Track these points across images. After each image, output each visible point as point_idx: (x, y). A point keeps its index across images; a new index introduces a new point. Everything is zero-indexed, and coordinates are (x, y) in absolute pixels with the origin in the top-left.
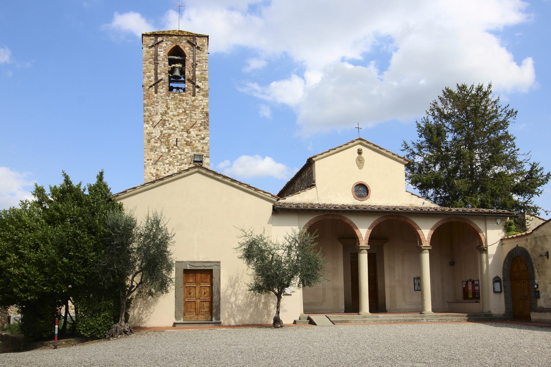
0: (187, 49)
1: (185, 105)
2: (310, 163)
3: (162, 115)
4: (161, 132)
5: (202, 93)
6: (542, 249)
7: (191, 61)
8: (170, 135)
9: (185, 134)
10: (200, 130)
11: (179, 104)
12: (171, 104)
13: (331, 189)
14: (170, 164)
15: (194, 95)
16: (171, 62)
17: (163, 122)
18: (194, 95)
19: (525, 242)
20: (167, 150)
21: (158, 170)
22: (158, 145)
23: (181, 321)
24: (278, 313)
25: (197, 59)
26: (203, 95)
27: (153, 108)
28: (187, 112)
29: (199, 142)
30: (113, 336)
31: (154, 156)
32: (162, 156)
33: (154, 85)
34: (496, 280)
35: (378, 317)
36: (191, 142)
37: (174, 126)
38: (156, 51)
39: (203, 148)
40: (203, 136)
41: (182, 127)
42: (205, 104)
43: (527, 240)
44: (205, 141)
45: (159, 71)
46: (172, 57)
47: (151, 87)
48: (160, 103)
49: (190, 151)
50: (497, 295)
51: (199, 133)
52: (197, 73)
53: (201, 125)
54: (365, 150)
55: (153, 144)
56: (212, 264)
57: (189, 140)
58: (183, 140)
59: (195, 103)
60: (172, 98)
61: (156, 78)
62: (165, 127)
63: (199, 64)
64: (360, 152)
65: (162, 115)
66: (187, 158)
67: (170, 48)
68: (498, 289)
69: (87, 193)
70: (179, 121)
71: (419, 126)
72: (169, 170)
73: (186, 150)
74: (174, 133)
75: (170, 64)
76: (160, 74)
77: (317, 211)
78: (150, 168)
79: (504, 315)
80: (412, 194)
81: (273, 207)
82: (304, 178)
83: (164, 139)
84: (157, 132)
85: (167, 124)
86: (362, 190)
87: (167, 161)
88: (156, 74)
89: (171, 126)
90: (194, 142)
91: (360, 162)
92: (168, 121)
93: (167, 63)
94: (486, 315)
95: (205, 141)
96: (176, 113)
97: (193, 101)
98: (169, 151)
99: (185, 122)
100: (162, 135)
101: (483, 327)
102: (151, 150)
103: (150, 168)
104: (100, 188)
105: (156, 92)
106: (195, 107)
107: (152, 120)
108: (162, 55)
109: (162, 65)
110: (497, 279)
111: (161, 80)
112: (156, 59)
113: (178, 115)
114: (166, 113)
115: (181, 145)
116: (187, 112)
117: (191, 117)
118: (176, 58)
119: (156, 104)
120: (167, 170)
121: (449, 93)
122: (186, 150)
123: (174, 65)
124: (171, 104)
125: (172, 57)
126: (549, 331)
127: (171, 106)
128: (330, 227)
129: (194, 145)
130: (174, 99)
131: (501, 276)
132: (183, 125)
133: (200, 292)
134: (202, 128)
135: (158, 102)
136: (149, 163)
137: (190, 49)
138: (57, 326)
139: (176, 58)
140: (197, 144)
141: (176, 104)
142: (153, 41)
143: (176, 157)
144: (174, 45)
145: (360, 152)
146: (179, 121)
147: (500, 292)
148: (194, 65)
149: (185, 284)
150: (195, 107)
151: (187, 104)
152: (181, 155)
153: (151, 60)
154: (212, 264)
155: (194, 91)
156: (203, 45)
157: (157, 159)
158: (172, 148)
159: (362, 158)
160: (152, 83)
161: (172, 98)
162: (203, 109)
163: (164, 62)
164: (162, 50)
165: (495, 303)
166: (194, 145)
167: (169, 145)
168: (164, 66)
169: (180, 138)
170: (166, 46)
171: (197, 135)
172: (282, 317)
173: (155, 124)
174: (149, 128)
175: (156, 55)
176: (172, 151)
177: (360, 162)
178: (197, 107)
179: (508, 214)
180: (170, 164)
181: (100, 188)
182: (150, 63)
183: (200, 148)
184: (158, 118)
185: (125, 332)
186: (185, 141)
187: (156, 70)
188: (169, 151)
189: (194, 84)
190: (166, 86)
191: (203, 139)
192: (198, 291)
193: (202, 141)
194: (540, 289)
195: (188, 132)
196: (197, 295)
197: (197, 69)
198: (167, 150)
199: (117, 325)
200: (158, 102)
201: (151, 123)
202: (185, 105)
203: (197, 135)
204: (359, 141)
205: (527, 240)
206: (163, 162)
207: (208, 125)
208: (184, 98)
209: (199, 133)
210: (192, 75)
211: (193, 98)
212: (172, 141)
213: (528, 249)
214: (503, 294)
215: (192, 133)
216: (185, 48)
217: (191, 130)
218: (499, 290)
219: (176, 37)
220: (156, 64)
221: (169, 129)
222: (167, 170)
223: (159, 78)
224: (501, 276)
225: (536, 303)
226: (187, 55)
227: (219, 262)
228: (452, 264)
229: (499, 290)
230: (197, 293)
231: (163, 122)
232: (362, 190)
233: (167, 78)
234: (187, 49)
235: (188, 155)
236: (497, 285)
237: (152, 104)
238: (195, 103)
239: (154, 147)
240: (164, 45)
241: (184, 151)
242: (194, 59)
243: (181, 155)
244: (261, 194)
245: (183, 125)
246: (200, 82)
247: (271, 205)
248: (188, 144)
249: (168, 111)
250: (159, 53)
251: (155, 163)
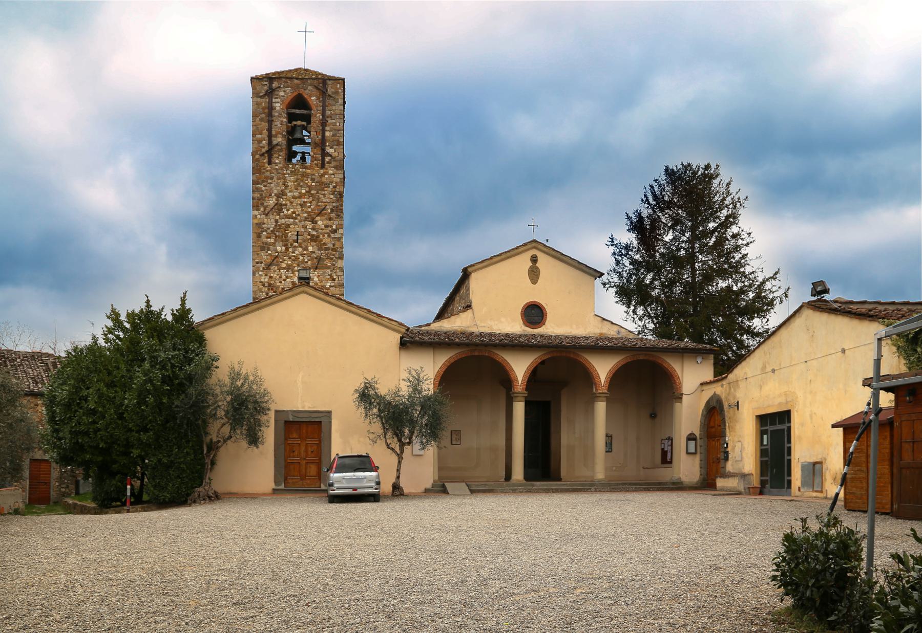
0: (314, 98)
1: (309, 182)
2: (466, 275)
3: (278, 196)
4: (277, 221)
5: (333, 164)
6: (734, 398)
7: (319, 116)
8: (288, 226)
9: (310, 225)
10: (330, 219)
11: (302, 181)
12: (291, 181)
13: (494, 311)
14: (289, 268)
15: (323, 166)
16: (291, 117)
17: (279, 208)
18: (323, 166)
19: (720, 388)
20: (284, 248)
21: (271, 277)
22: (272, 241)
23: (282, 487)
24: (398, 477)
25: (328, 113)
26: (336, 168)
27: (265, 186)
28: (313, 192)
29: (329, 236)
30: (195, 502)
31: (265, 257)
32: (277, 257)
33: (267, 152)
34: (691, 438)
35: (533, 486)
36: (318, 237)
37: (294, 212)
38: (271, 103)
39: (334, 245)
40: (334, 227)
41: (305, 215)
42: (338, 180)
43: (722, 386)
44: (337, 235)
45: (273, 133)
46: (293, 111)
47: (262, 155)
48: (275, 179)
49: (316, 249)
50: (691, 457)
51: (329, 223)
52: (327, 134)
53: (332, 211)
54: (541, 257)
55: (265, 240)
56: (321, 415)
57: (314, 233)
58: (306, 234)
59: (324, 179)
60: (292, 172)
61: (270, 142)
62: (282, 214)
63: (330, 121)
64: (534, 260)
65: (278, 196)
66: (312, 259)
67: (290, 98)
68: (692, 449)
69: (170, 318)
70: (301, 205)
71: (629, 218)
72: (287, 277)
73: (310, 249)
74: (295, 224)
75: (290, 121)
76: (276, 136)
77: (458, 345)
78: (261, 275)
79: (697, 483)
80: (604, 319)
81: (401, 338)
82: (456, 298)
83: (280, 232)
84: (270, 223)
85: (284, 210)
86: (534, 313)
87: (284, 265)
88: (270, 136)
89: (289, 212)
90: (321, 237)
91: (534, 274)
92: (286, 205)
93: (285, 120)
94: (674, 483)
95: (337, 235)
96: (296, 194)
97: (323, 175)
98: (287, 250)
99: (310, 207)
100: (278, 226)
101: (680, 499)
102: (262, 249)
103: (261, 275)
104: (183, 315)
105: (270, 163)
106: (322, 185)
107: (262, 204)
108: (278, 108)
109: (278, 124)
110: (692, 437)
111: (277, 145)
112: (270, 114)
113: (300, 197)
114: (283, 194)
115: (304, 241)
116: (313, 192)
117: (319, 199)
118: (297, 111)
119: (270, 181)
120: (284, 277)
121: (669, 172)
122: (310, 249)
123: (295, 123)
124: (291, 181)
125: (293, 111)
126: (920, 523)
127: (290, 184)
128: (473, 366)
129: (321, 240)
130: (293, 173)
131: (697, 433)
132: (307, 212)
133: (306, 451)
134: (333, 215)
135: (272, 178)
136: (259, 268)
137: (318, 98)
138: (129, 487)
139: (297, 111)
140: (326, 240)
141: (297, 179)
142: (266, 88)
143: (296, 258)
144: (296, 94)
145: (534, 260)
146: (301, 205)
147: (695, 453)
148: (324, 124)
149: (286, 439)
150: (322, 185)
151: (313, 180)
152: (303, 255)
153: (263, 116)
154: (321, 415)
155: (323, 160)
156: (337, 93)
157: (269, 261)
158: (292, 245)
159: (537, 268)
160: (264, 150)
161: (292, 172)
162: (335, 187)
163: (281, 119)
164: (278, 100)
165: (687, 467)
166: (321, 240)
167: (287, 241)
168: (280, 123)
169: (303, 230)
170: (285, 94)
171: (326, 226)
172: (403, 483)
173: (268, 209)
174: (259, 217)
175: (271, 108)
176: (291, 250)
177: (534, 274)
178: (327, 185)
179: (710, 350)
180: (289, 268)
181: (183, 315)
182: (261, 120)
183: (330, 245)
184: (272, 202)
185: (210, 498)
186: (309, 234)
187: (270, 130)
188: (287, 250)
189: (323, 150)
190: (283, 154)
191: (335, 231)
192: (303, 449)
193: (332, 235)
194: (729, 449)
195: (314, 222)
196: (303, 454)
197: (327, 128)
198: (284, 248)
199: (201, 489)
200: (272, 178)
201: (262, 209)
202: (309, 182)
203: (326, 226)
204: (534, 244)
205: (722, 386)
206: (277, 265)
207: (342, 211)
208: (308, 171)
209: (329, 223)
210: (320, 137)
211: (322, 171)
212: (291, 235)
213: (723, 397)
214: (698, 457)
215: (320, 223)
216: (310, 96)
217: (318, 218)
218: (693, 451)
219: (298, 82)
220: (270, 122)
221: (287, 217)
222: (284, 277)
223: (275, 142)
224: (697, 433)
225: (724, 467)
226: (314, 108)
227: (330, 412)
228: (653, 416)
229: (693, 451)
230: (302, 452)
231: (279, 208)
232: (534, 313)
233: (285, 142)
234: (313, 100)
235: (314, 255)
236: (692, 444)
237: (263, 181)
238: (324, 179)
239: (266, 243)
240: (282, 93)
241: (306, 249)
242: (323, 114)
243: (303, 255)
244: (386, 322)
245: (307, 212)
246: (332, 148)
247: (398, 336)
248: (314, 239)
249: (287, 191)
250: (274, 105)
251: (268, 267)
